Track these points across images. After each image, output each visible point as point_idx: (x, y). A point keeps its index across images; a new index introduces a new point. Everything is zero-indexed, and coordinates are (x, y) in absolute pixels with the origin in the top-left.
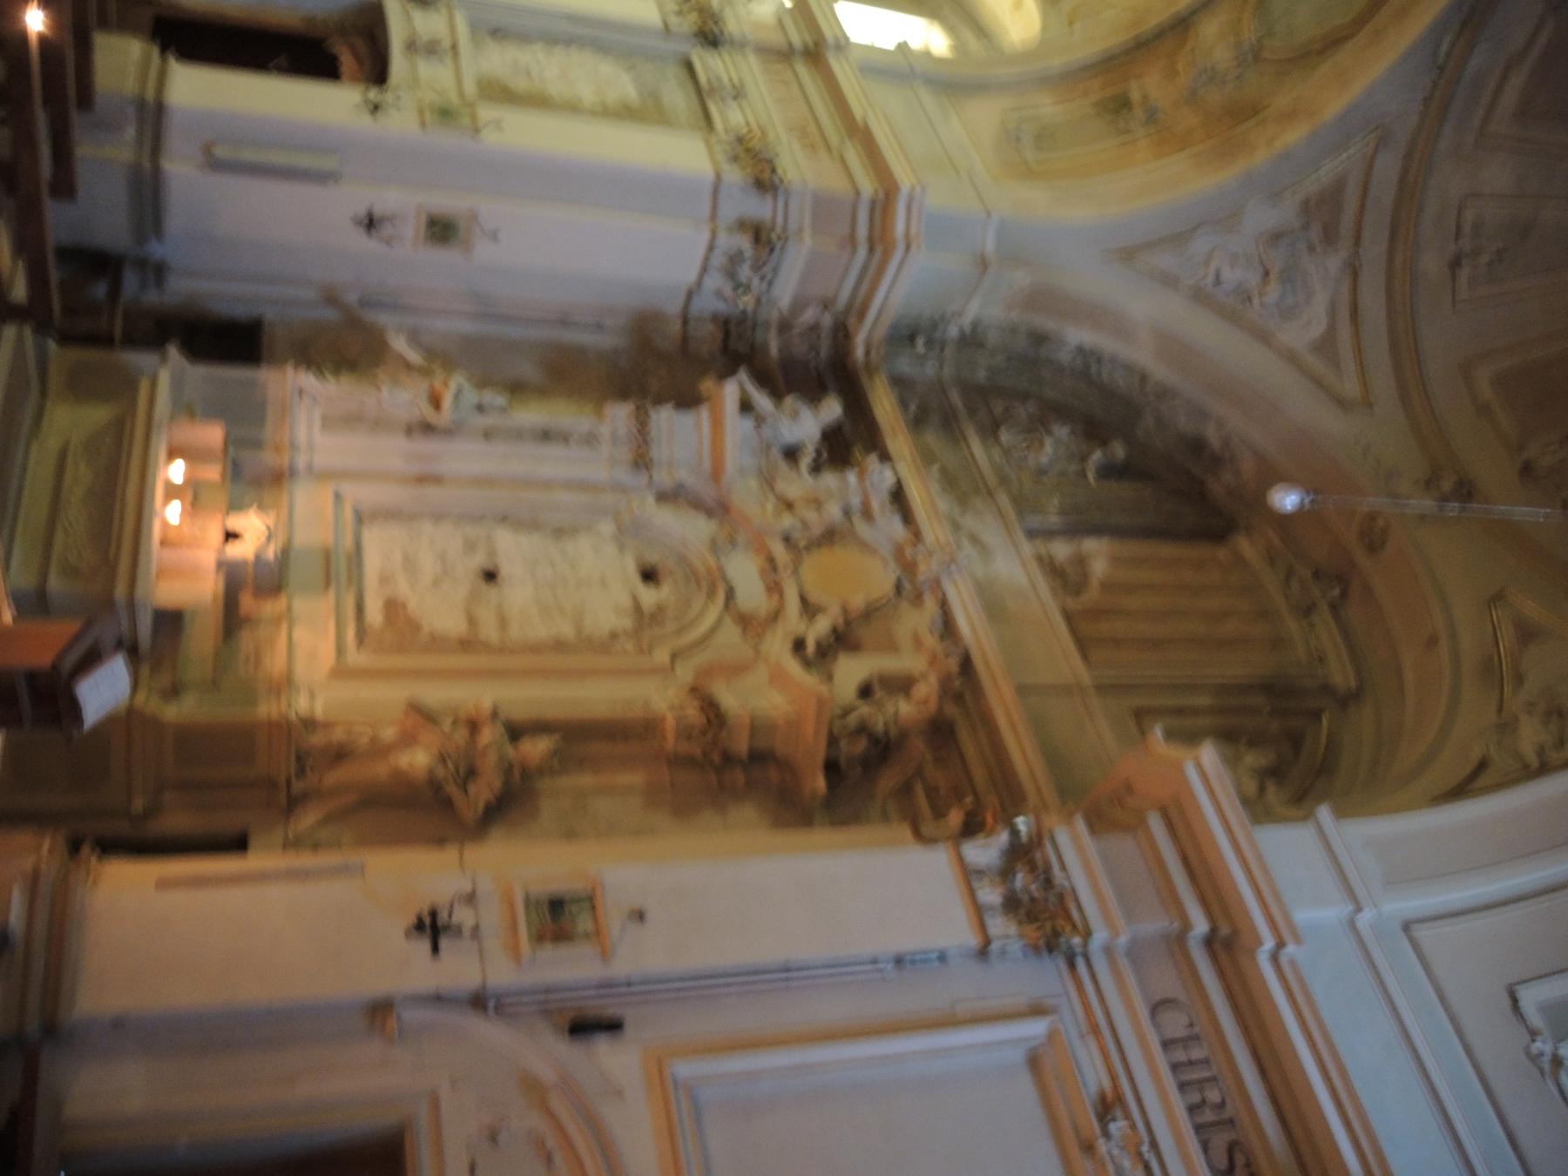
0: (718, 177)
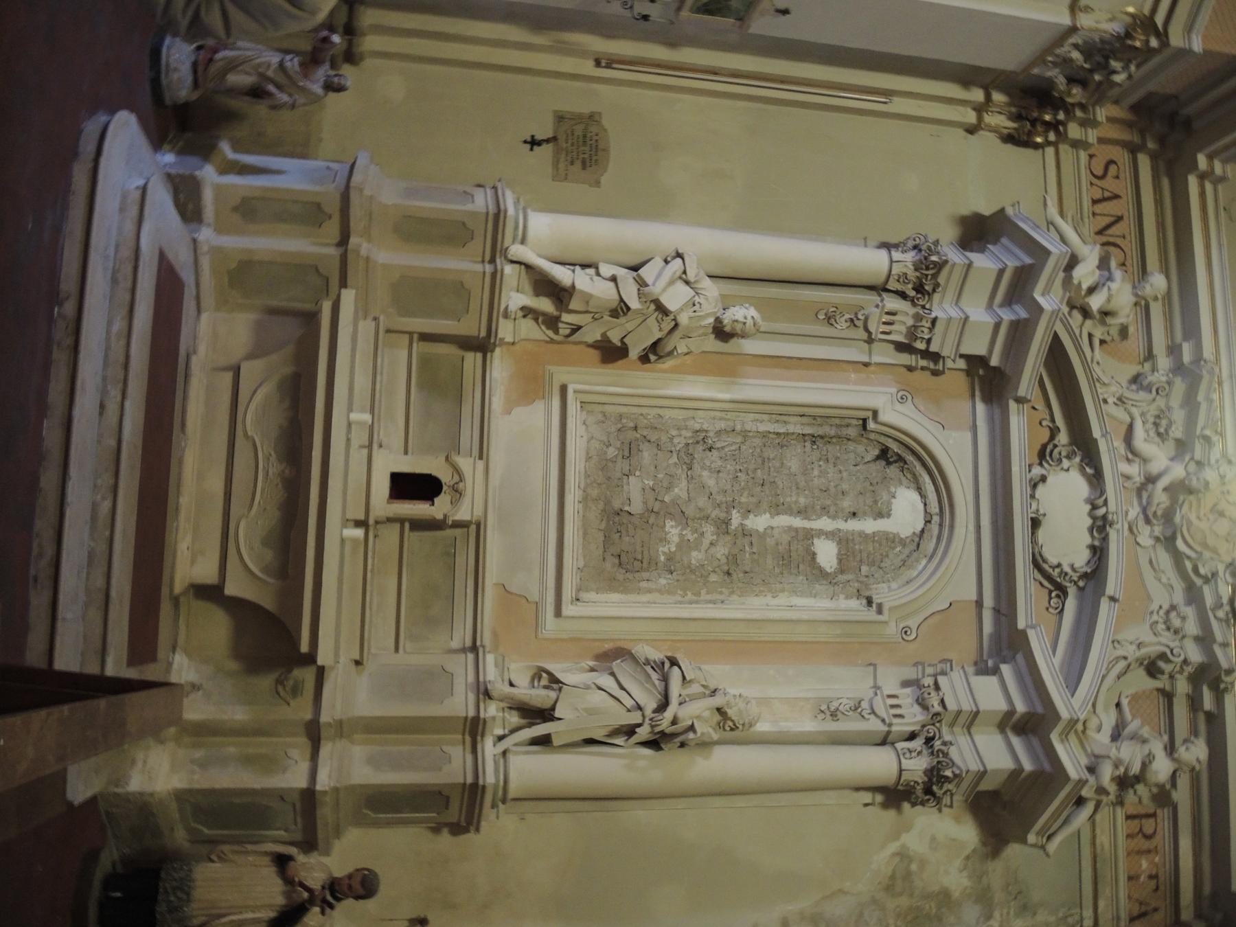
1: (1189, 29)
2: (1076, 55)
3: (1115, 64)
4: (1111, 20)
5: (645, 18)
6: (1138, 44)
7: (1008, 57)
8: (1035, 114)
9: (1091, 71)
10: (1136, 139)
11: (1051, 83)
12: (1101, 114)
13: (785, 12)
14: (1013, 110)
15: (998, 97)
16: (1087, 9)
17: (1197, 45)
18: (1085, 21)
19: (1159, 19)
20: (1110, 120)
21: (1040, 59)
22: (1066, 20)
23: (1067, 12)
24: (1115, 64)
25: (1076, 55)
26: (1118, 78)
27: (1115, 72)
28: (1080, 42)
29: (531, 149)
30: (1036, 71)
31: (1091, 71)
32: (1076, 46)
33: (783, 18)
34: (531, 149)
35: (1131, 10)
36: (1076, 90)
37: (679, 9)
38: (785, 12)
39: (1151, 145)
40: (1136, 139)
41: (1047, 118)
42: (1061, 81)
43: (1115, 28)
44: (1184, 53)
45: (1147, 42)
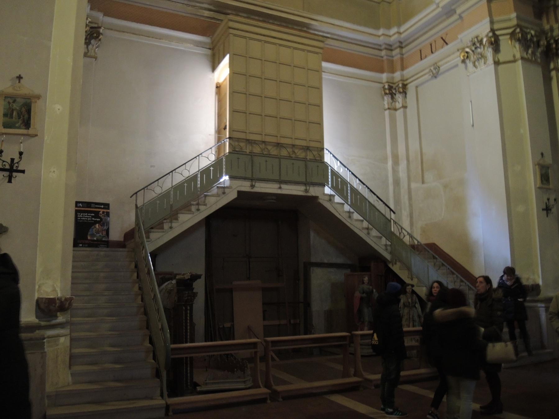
0: (389, 109)
1: (510, 20)
2: (530, 51)
3: (529, 36)
4: (515, 47)
5: (555, 200)
6: (520, 35)
7: (537, 72)
8: (554, 51)
9: (533, 42)
10: (552, 9)
11: (541, 54)
12: (547, 27)
13: (542, 154)
14: (555, 58)
15: (552, 66)
16: (514, 56)
17: (514, 15)
18: (518, 56)
19: (510, 31)
20: (548, 22)
21: (535, 62)
22: (520, 62)
23: (517, 63)
24: (529, 36)
25: (530, 51)
26: (533, 32)
27: (532, 35)
28: (525, 53)
29: (543, 210)
30: (539, 60)
31: (533, 42)
32: (527, 54)
33: (545, 154)
34: (543, 210)
35: (510, 42)
36: (542, 43)
37: (550, 189)
38: (542, 154)
39: (552, 3)
40: (552, 9)
41: (554, 46)
42: (540, 50)
43: (517, 45)
44: (518, 17)
45: (518, 33)
